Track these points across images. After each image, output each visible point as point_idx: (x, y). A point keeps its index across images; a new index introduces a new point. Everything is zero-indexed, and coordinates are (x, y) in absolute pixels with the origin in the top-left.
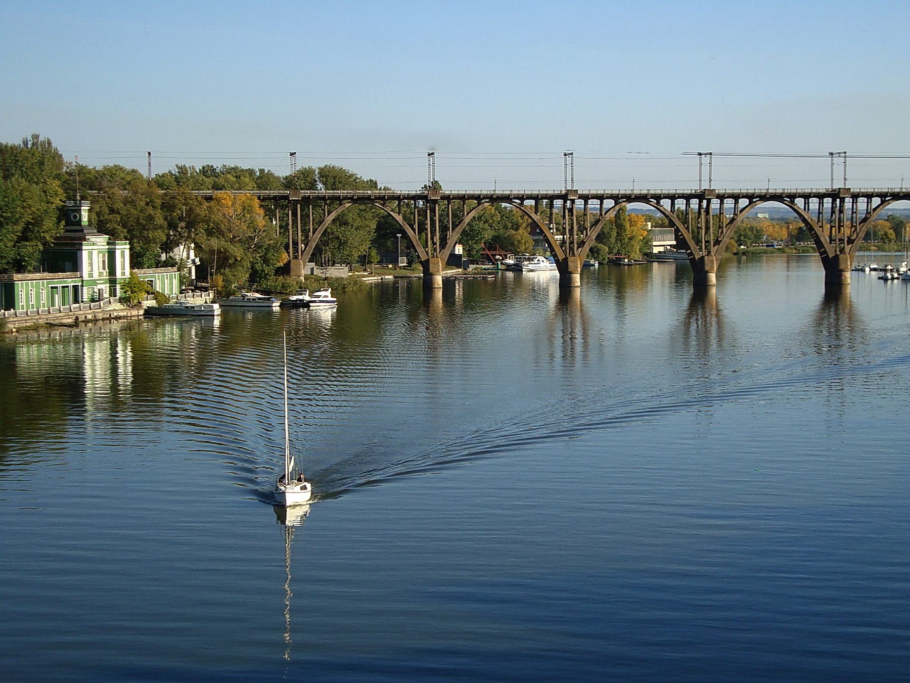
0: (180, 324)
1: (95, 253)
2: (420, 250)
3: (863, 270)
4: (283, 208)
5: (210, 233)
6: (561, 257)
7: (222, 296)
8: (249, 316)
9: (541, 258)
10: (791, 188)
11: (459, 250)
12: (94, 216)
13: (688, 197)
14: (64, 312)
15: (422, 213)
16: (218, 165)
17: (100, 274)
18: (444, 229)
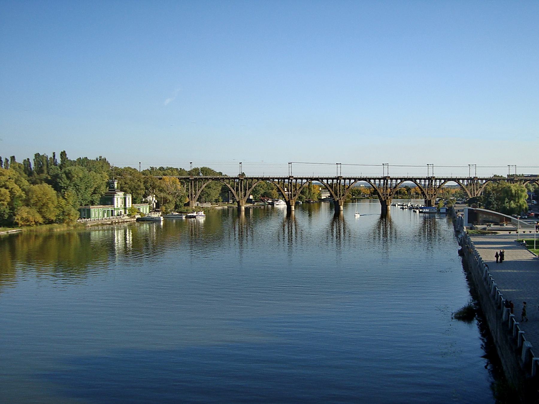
0: (149, 224)
1: (119, 198)
2: (236, 197)
3: (395, 205)
4: (188, 182)
5: (161, 191)
6: (287, 200)
7: (164, 214)
8: (174, 221)
9: (281, 200)
10: (369, 176)
11: (251, 197)
12: (119, 185)
13: (333, 179)
14: (107, 219)
15: (238, 184)
16: (165, 167)
17: (121, 206)
18: (245, 190)
